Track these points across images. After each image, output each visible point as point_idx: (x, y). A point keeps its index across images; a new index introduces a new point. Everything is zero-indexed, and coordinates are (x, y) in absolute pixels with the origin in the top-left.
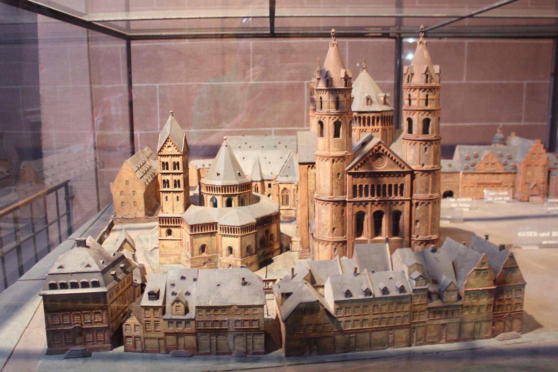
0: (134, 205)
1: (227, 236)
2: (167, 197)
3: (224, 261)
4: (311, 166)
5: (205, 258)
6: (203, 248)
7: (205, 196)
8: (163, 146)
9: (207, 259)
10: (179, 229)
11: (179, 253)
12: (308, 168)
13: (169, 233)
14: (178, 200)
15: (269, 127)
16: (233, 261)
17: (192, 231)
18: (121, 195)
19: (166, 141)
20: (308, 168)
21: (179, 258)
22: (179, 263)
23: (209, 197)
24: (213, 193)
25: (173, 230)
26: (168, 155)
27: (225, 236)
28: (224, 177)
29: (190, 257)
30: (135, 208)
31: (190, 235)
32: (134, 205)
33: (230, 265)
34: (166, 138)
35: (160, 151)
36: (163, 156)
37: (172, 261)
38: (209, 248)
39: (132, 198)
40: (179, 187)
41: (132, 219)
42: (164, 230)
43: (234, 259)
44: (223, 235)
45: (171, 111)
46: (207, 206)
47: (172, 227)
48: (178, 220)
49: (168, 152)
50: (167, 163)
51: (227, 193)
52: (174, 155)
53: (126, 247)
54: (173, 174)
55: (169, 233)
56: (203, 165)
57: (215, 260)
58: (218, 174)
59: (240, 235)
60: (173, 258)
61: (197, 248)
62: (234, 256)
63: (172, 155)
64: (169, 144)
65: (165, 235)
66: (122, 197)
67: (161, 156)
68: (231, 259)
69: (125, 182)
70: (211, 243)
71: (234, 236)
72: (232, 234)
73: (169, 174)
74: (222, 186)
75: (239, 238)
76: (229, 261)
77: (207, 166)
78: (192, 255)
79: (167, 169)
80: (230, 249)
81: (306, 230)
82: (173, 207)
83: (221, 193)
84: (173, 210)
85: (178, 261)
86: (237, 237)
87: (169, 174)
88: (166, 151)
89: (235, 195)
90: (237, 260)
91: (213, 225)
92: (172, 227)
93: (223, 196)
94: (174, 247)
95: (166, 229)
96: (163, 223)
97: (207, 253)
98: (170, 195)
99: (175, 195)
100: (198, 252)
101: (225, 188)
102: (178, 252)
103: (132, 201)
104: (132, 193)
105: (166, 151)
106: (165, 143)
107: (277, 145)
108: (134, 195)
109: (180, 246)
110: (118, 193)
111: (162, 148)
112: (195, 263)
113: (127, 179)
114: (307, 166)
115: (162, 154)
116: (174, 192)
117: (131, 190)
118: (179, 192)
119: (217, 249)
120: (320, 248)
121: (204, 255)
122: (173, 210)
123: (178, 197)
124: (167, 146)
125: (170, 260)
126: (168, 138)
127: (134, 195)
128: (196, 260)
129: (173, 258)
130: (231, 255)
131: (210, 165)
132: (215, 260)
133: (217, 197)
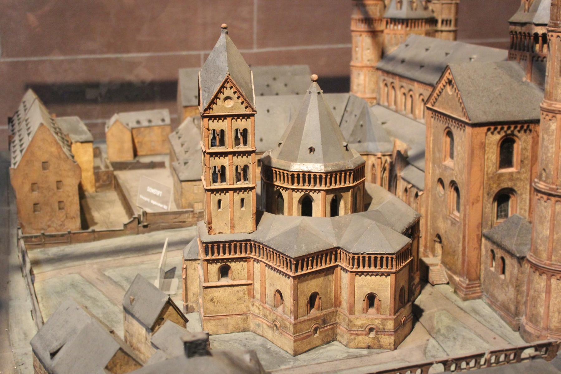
0: (60, 209)
1: (367, 273)
2: (219, 201)
3: (359, 323)
4: (492, 128)
5: (316, 319)
6: (312, 300)
7: (285, 194)
8: (216, 97)
9: (320, 321)
10: (245, 264)
11: (245, 310)
12: (486, 134)
13: (224, 271)
14: (242, 206)
15: (195, 49)
16: (377, 322)
17: (207, 254)
18: (33, 190)
19: (223, 87)
20: (486, 134)
21: (245, 320)
22: (244, 330)
23: (297, 196)
24: (305, 187)
25: (233, 265)
26: (225, 117)
27: (362, 273)
28: (325, 154)
29: (293, 322)
30: (61, 215)
31: (294, 278)
32: (60, 209)
33: (371, 330)
34: (223, 80)
35: (209, 108)
36: (219, 117)
37: (230, 328)
38: (323, 298)
39: (54, 194)
40: (223, 180)
41: (62, 235)
42: (214, 268)
43: (380, 316)
44: (357, 273)
45: (224, 25)
46: (290, 213)
47: (233, 260)
48: (246, 247)
49: (226, 109)
50: (222, 132)
51: (333, 187)
52: (238, 116)
53: (170, 315)
54: (234, 154)
55: (224, 271)
56: (138, 122)
57: (333, 321)
58: (311, 150)
59: (394, 270)
60: (232, 322)
61: (303, 301)
62: (378, 310)
63: (233, 117)
64: (228, 92)
65: (216, 277)
66: (35, 193)
67: (210, 118)
68: (372, 317)
69: (41, 165)
70: (326, 287)
71: (382, 274)
72: (378, 269)
73: (225, 154)
74: (326, 173)
75: (393, 276)
76: (369, 322)
77: (145, 123)
78: (296, 318)
79: (222, 143)
80: (371, 299)
81: (477, 246)
82: (232, 220)
83: (323, 188)
84: (233, 227)
85: (241, 326)
86: (388, 274)
87: (225, 154)
88: (219, 108)
89: (347, 189)
90: (385, 320)
91: (332, 253)
92: (233, 260)
93: (328, 192)
94: (235, 299)
95: (219, 265)
96: (213, 254)
97: (318, 309)
98: (226, 198)
99: (237, 197)
100: (305, 309)
101: (331, 175)
102: (242, 308)
103: (54, 201)
104: (54, 186)
105: (219, 108)
106: (220, 91)
107: (271, 82)
108: (58, 188)
109: (247, 297)
110: (27, 187)
111: (213, 102)
112: (301, 330)
113: (45, 157)
114: (485, 128)
115: (211, 113)
116: (235, 190)
117: (53, 179)
118: (245, 189)
119: (336, 298)
120: (553, 286)
121: (314, 312)
122: (233, 227)
123: (242, 200)
124: (222, 96)
125: (226, 326)
126: (226, 81)
127: (58, 188)
128: (302, 326)
129: (232, 322)
130: (372, 310)
131: (150, 121)
132: (333, 321)
133: (313, 195)
